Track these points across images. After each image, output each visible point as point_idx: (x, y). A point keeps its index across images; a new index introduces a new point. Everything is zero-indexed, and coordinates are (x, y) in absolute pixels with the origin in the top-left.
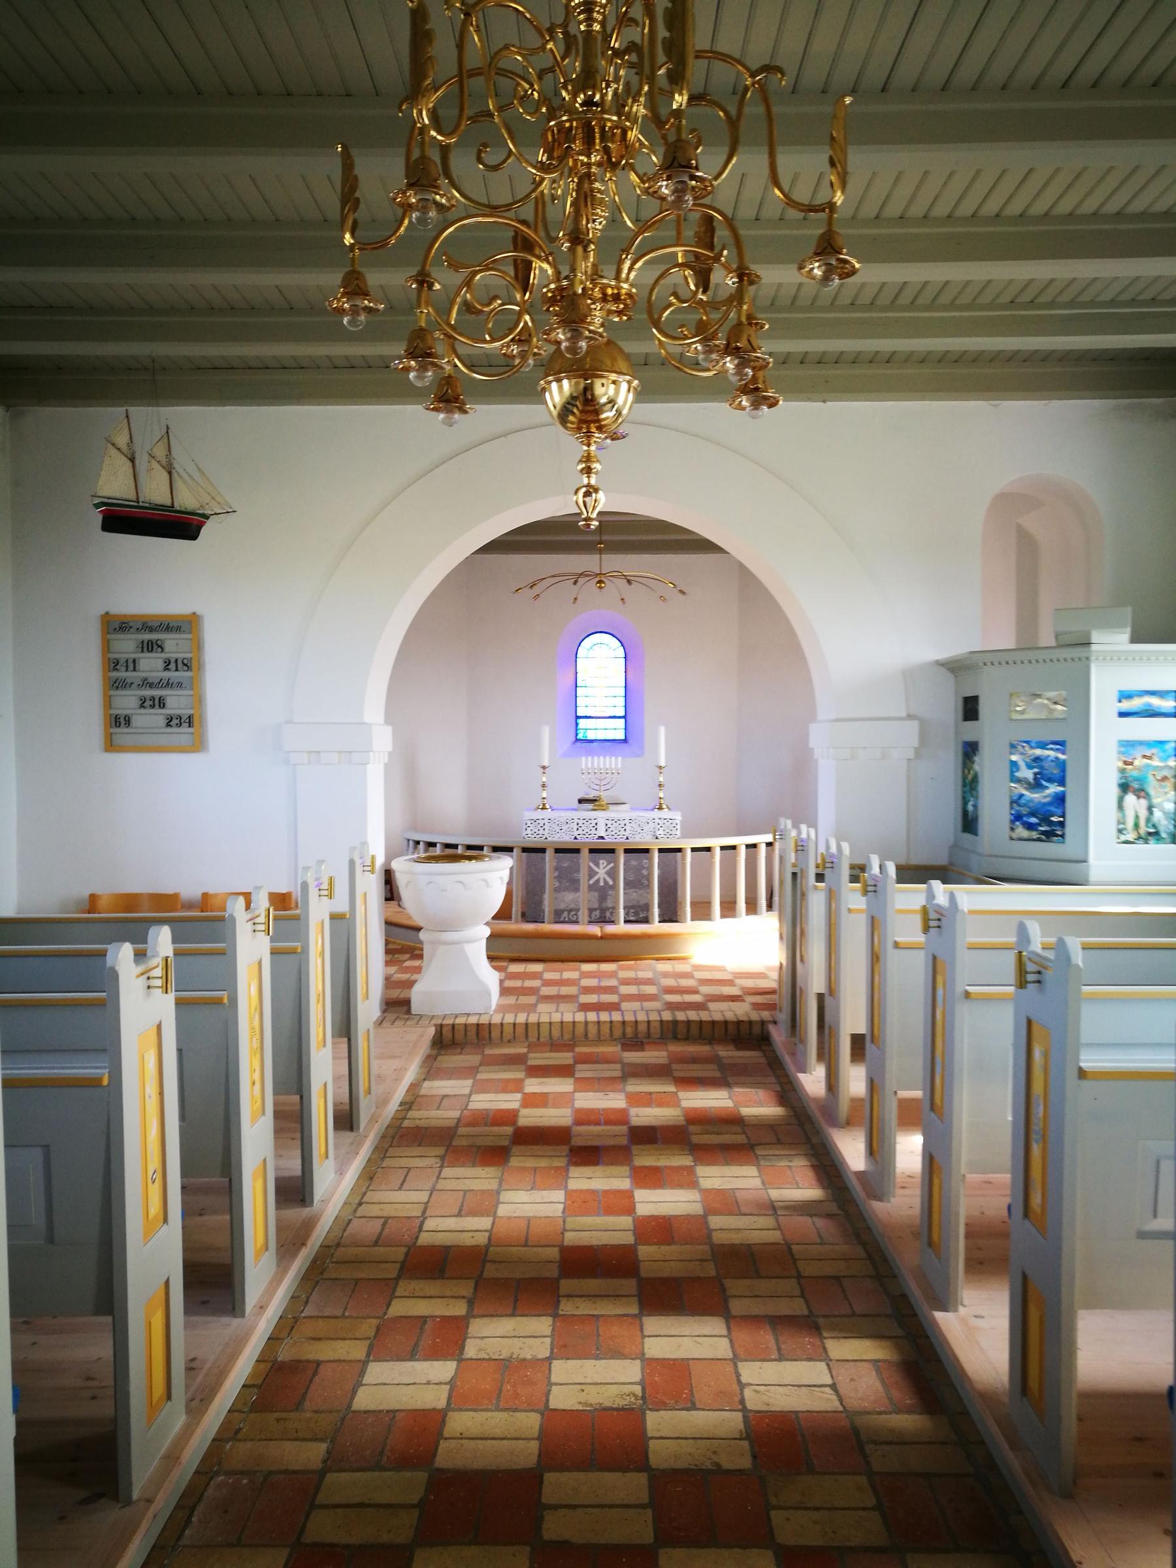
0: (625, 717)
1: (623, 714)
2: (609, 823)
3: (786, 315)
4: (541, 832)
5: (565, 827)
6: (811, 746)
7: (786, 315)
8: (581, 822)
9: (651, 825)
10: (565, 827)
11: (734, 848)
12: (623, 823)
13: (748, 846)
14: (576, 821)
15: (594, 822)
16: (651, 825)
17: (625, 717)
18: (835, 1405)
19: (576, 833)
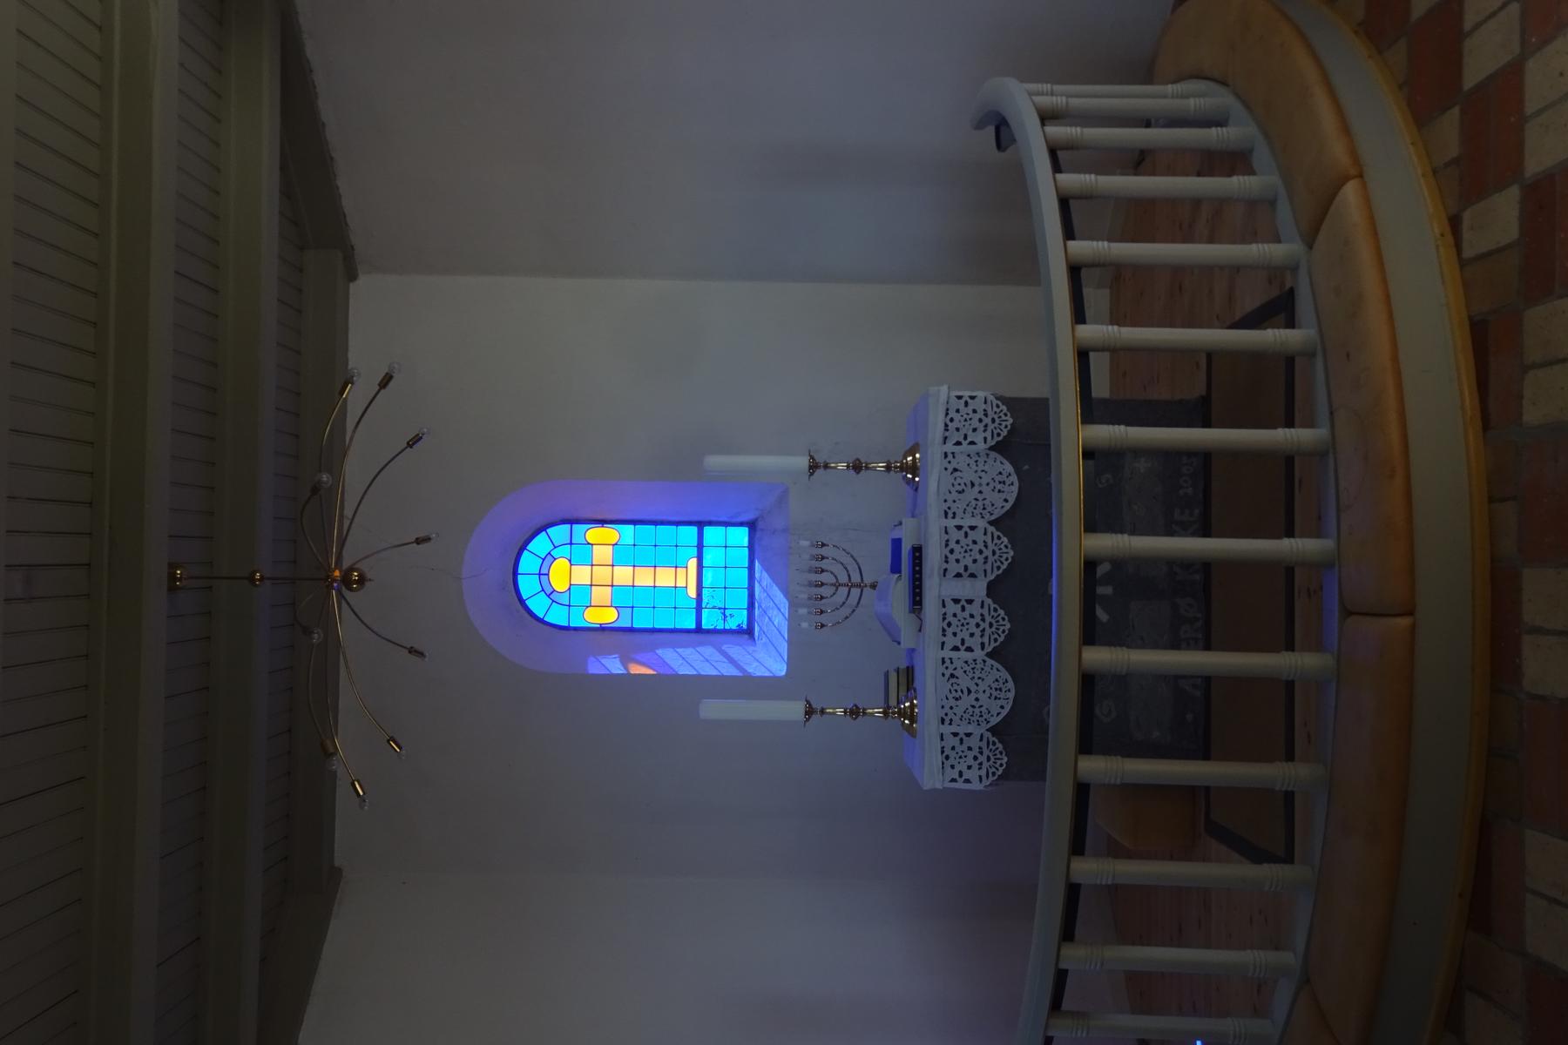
0: (699, 629)
1: (705, 625)
2: (954, 568)
3: (117, 38)
4: (974, 742)
5: (965, 682)
6: (337, 864)
7: (117, 38)
8: (951, 641)
9: (961, 461)
10: (965, 682)
11: (1064, 203)
12: (955, 535)
13: (1057, 168)
14: (947, 653)
15: (952, 608)
16: (961, 461)
17: (699, 629)
18: (1530, 107)
19: (979, 654)
